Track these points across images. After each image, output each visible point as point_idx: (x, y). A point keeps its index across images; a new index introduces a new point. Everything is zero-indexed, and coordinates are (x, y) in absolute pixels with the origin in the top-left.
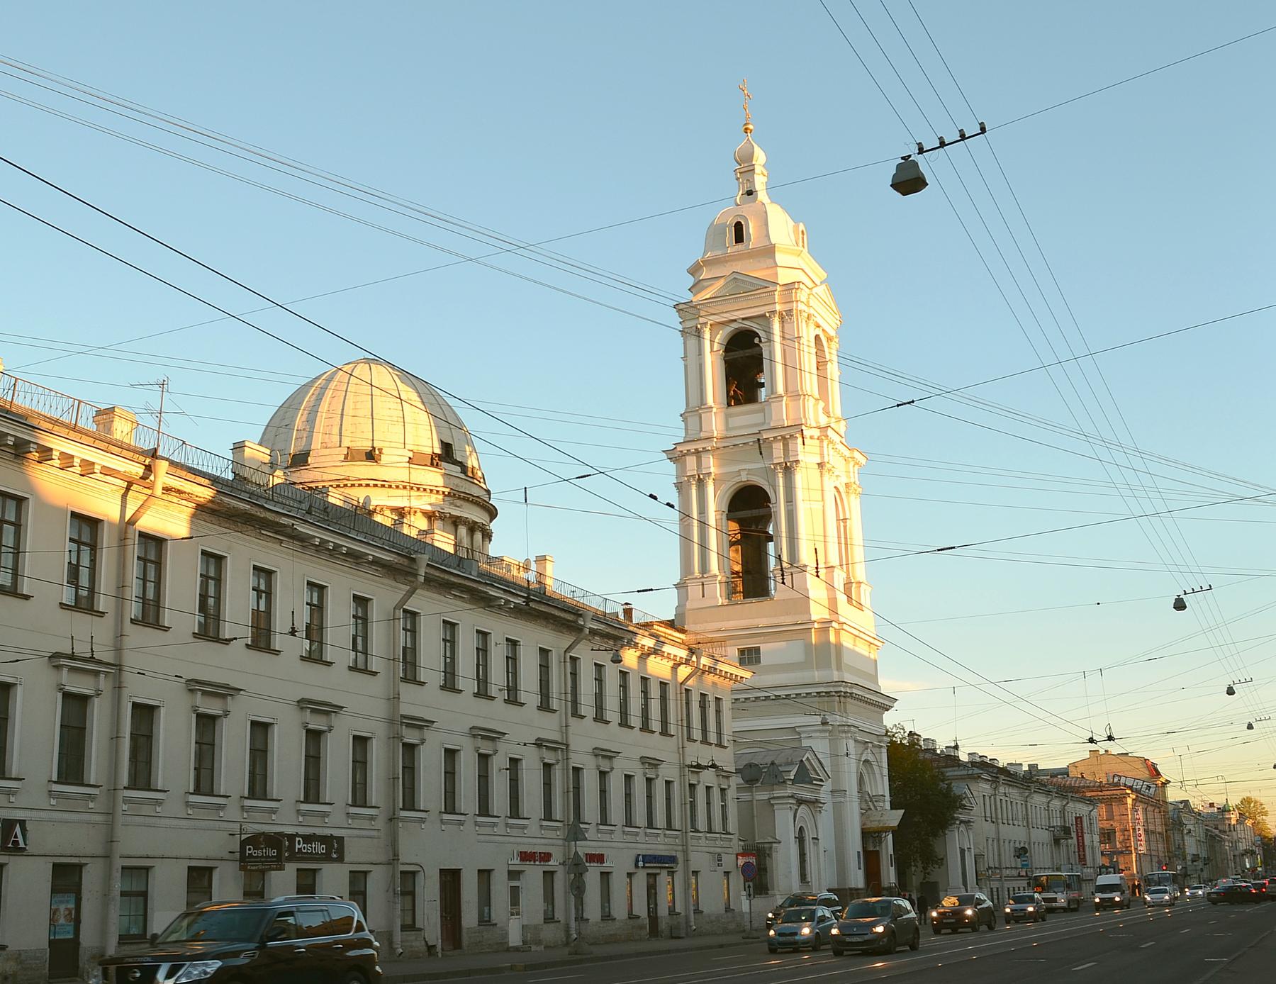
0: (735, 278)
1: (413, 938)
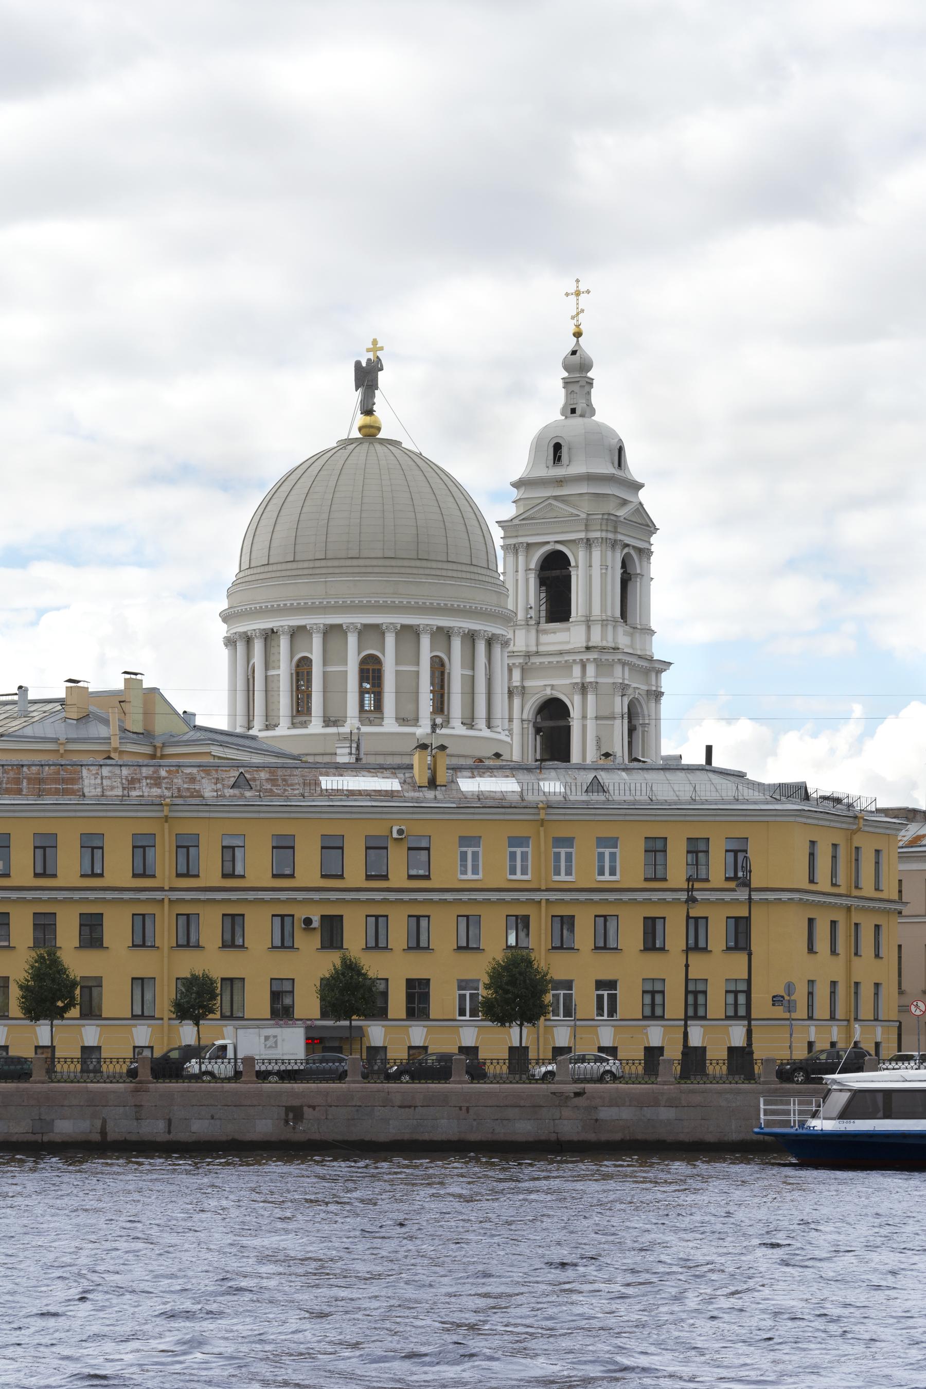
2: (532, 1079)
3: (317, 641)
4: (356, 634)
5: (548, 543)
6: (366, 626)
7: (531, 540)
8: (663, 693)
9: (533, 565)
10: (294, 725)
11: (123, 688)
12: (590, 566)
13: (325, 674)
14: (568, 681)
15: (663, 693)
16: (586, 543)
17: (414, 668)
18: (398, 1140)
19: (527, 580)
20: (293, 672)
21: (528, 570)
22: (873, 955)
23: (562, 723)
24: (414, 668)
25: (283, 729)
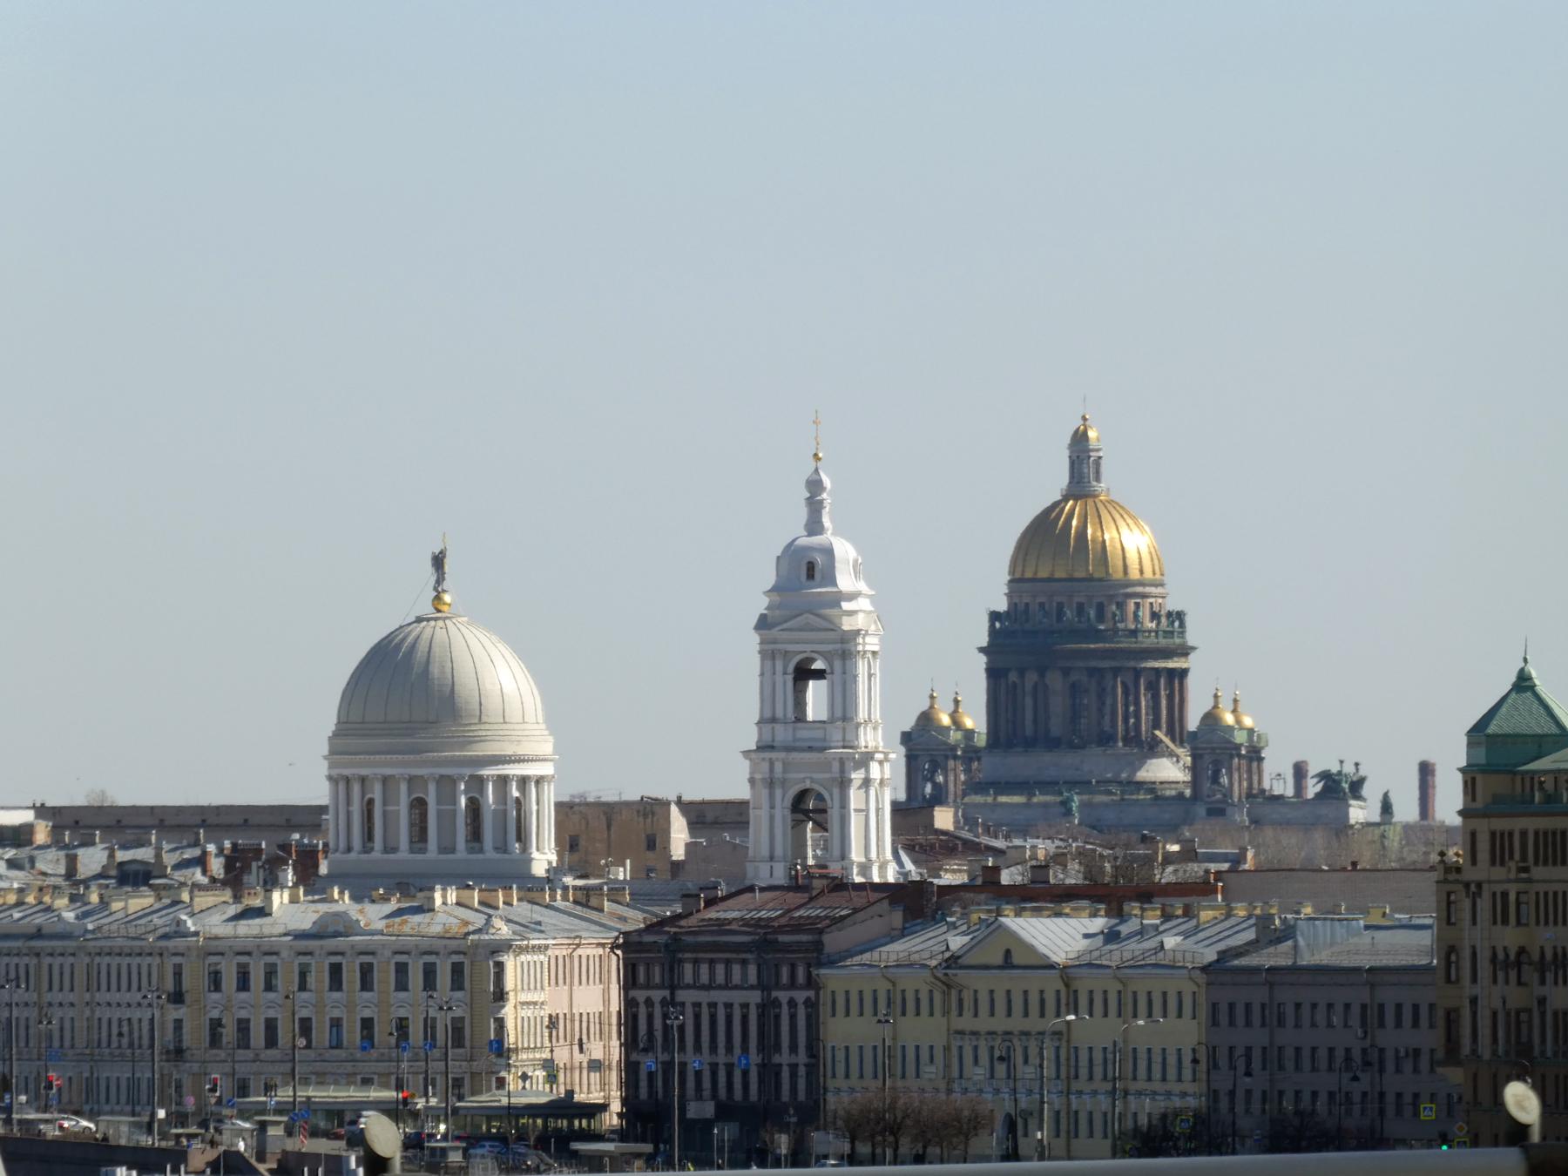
2: (657, 1071)
3: (432, 788)
4: (434, 784)
6: (442, 776)
8: (1263, 758)
10: (412, 851)
11: (674, 858)
12: (844, 673)
13: (385, 814)
14: (827, 776)
15: (1263, 758)
16: (785, 656)
17: (452, 807)
18: (202, 807)
19: (785, 683)
20: (365, 809)
21: (785, 673)
22: (1079, 992)
24: (452, 807)
25: (404, 853)
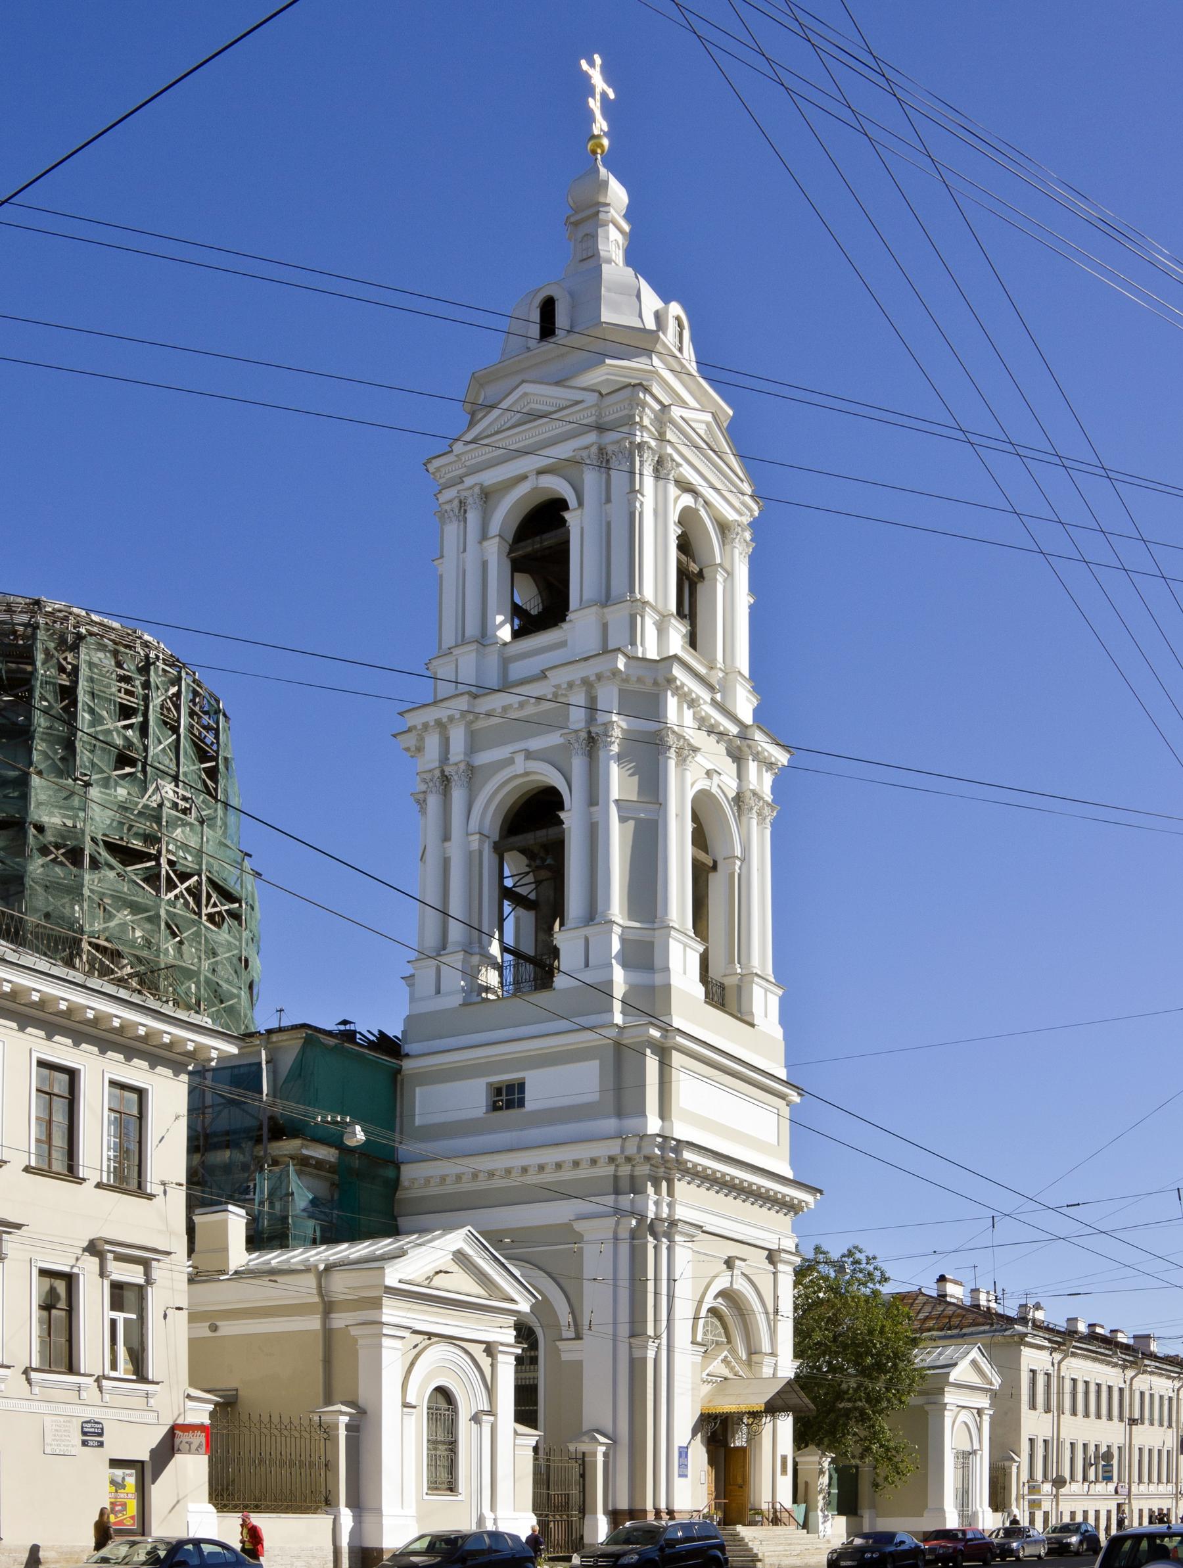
0: (525, 394)
1: (411, 1399)
5: (524, 478)
7: (490, 477)
9: (495, 527)
21: (484, 536)
23: (552, 831)
